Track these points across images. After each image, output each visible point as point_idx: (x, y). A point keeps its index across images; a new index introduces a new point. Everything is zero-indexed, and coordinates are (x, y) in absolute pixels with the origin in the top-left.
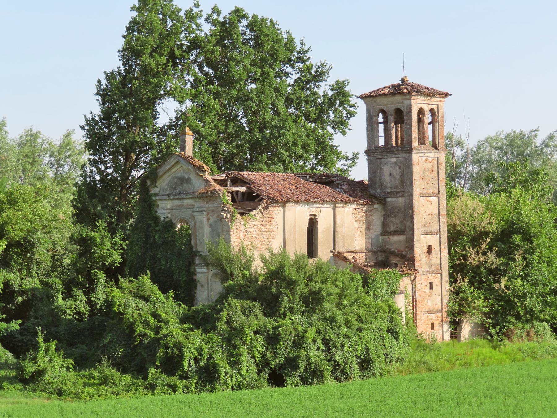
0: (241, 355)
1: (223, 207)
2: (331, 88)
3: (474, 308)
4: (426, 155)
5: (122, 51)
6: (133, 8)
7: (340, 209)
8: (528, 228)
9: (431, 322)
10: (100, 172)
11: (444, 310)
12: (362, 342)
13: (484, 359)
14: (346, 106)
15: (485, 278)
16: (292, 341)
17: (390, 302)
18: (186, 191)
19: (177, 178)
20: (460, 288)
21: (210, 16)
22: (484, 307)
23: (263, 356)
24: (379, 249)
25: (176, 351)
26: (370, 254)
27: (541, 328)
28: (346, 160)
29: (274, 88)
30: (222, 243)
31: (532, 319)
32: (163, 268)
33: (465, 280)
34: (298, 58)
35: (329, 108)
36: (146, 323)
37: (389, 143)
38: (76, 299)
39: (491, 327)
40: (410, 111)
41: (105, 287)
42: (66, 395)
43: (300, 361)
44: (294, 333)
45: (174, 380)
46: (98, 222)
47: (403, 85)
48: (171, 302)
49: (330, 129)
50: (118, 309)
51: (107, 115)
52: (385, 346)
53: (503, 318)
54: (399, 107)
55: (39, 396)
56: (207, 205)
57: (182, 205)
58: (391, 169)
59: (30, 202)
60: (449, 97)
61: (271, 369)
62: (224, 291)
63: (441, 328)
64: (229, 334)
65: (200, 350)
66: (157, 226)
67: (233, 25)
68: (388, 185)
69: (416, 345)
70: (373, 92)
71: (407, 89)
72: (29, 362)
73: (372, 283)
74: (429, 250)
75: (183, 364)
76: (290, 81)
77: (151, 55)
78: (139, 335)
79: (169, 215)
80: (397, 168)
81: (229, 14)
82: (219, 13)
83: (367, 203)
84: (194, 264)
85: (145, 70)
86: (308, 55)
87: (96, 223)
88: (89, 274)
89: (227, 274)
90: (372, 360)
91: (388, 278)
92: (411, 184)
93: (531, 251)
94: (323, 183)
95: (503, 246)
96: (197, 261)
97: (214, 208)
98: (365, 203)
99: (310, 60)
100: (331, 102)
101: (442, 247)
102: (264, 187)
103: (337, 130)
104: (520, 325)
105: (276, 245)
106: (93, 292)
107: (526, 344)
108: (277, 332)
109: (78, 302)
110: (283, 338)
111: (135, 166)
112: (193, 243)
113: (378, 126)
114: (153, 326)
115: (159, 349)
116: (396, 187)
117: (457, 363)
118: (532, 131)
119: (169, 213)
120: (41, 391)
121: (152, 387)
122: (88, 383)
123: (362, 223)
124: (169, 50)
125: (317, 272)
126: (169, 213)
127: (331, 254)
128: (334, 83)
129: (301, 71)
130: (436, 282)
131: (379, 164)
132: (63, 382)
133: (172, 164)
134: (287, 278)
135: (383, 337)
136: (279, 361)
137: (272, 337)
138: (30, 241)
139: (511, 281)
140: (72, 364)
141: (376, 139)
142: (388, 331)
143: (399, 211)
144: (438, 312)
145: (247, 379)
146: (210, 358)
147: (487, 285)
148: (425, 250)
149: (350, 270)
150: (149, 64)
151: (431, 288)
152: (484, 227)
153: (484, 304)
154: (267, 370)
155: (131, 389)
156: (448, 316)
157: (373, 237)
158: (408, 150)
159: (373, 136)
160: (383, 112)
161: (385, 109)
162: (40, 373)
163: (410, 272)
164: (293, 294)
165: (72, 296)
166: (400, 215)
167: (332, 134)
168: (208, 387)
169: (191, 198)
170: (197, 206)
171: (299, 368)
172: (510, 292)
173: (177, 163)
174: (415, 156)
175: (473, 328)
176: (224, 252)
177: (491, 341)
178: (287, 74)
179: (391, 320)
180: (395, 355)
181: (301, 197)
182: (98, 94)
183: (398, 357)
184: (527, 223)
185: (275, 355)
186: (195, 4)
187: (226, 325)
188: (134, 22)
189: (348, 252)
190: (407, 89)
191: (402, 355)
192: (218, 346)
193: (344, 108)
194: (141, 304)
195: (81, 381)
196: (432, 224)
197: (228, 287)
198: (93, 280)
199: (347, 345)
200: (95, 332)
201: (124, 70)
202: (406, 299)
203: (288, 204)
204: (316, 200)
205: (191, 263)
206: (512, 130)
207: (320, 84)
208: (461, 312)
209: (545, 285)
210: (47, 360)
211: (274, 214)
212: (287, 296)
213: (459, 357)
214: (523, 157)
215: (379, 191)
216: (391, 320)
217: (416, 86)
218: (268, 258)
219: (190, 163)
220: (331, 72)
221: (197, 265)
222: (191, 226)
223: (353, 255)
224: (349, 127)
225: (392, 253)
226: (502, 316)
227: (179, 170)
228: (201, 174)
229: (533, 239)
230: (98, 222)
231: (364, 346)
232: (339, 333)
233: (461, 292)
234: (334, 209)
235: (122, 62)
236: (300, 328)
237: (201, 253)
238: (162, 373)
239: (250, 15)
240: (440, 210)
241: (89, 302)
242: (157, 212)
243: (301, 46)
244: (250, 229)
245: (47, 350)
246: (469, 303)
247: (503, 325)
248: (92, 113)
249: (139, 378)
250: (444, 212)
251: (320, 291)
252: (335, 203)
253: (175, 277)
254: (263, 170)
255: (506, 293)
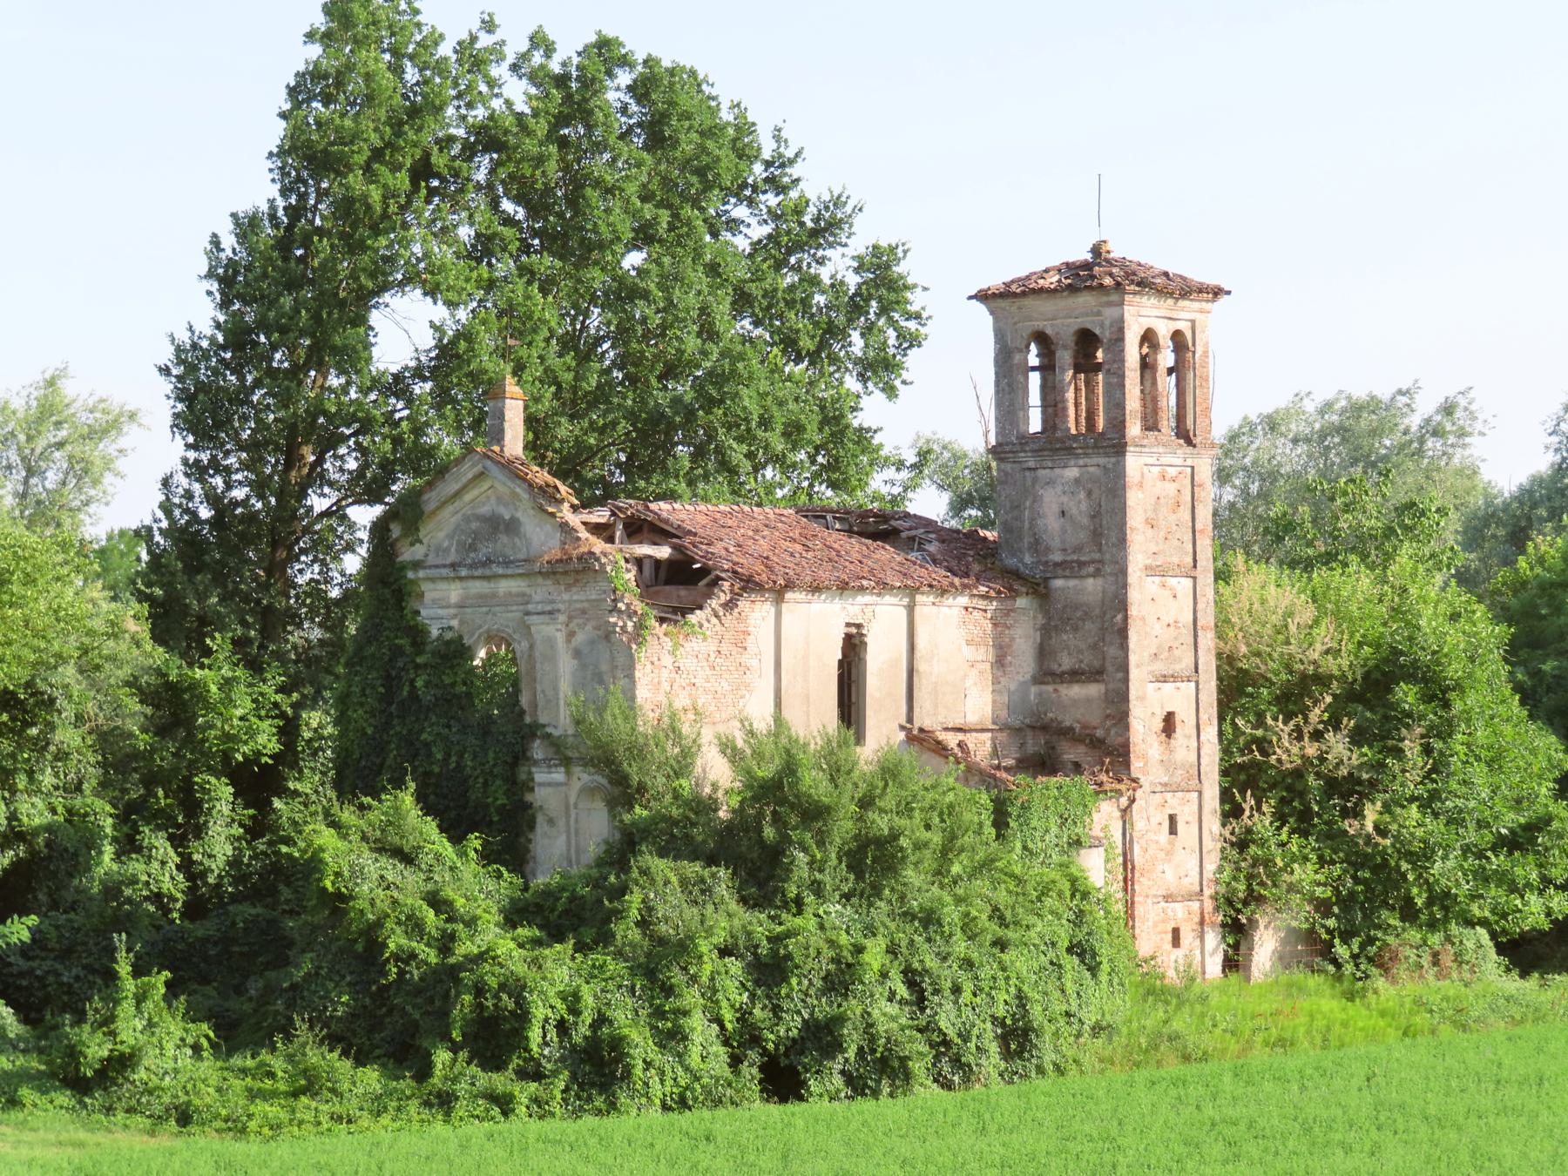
0: (686, 1013)
1: (614, 601)
2: (856, 264)
3: (1292, 888)
4: (1164, 460)
5: (278, 155)
6: (310, 36)
7: (926, 610)
8: (1439, 664)
9: (1172, 925)
10: (213, 499)
11: (1208, 892)
12: (1007, 978)
13: (1328, 1029)
14: (896, 316)
15: (1318, 803)
16: (823, 974)
17: (1073, 870)
18: (505, 556)
19: (479, 518)
20: (1249, 831)
21: (525, 57)
22: (1319, 884)
23: (743, 1016)
24: (1028, 721)
25: (508, 1002)
26: (1002, 736)
27: (1470, 945)
28: (898, 470)
29: (705, 266)
30: (614, 707)
31: (1446, 920)
32: (436, 769)
33: (1265, 808)
34: (766, 180)
35: (850, 320)
36: (414, 926)
37: (1060, 425)
38: (150, 857)
39: (1337, 941)
40: (1119, 338)
41: (229, 825)
42: (203, 1124)
43: (845, 1031)
44: (828, 953)
45: (500, 1081)
46: (213, 638)
47: (1099, 265)
48: (473, 865)
49: (852, 383)
50: (333, 883)
51: (237, 337)
52: (1063, 991)
53: (1365, 916)
54: (1089, 326)
55: (126, 1126)
56: (566, 597)
57: (494, 595)
58: (1065, 499)
59: (41, 582)
60: (1224, 300)
61: (765, 1052)
62: (618, 836)
63: (1198, 942)
64: (649, 955)
65: (573, 1001)
66: (420, 653)
67: (589, 84)
68: (1056, 543)
69: (1141, 990)
70: (1013, 282)
71: (1111, 275)
72: (94, 1031)
73: (1019, 816)
74: (1169, 724)
75: (527, 1038)
76: (742, 243)
77: (367, 168)
78: (396, 957)
79: (455, 623)
80: (1082, 495)
81: (579, 54)
82: (549, 50)
83: (999, 592)
84: (528, 759)
85: (347, 207)
86: (795, 171)
87: (208, 641)
88: (188, 781)
89: (629, 786)
90: (1034, 1030)
91: (1062, 801)
92: (1122, 541)
93: (1444, 731)
94: (876, 536)
95: (1368, 714)
96: (538, 750)
97: (586, 605)
98: (993, 594)
99: (801, 185)
100: (856, 306)
101: (1204, 717)
102: (720, 545)
103: (870, 384)
104: (1414, 935)
105: (761, 714)
106: (198, 837)
107: (1434, 988)
108: (782, 951)
109: (155, 865)
110: (797, 967)
111: (316, 477)
112: (524, 700)
113: (1027, 378)
114: (434, 932)
115: (458, 995)
116: (1078, 549)
117: (1259, 1038)
118: (1400, 392)
119: (454, 616)
120: (128, 1111)
121: (444, 1102)
122: (259, 1089)
123: (982, 650)
124: (418, 154)
125: (886, 785)
126: (454, 616)
127: (902, 736)
128: (862, 251)
129: (775, 216)
130: (1187, 813)
131: (1029, 482)
132: (189, 1086)
133: (464, 480)
134: (804, 800)
135: (1060, 966)
136: (788, 1030)
137: (766, 965)
138: (42, 693)
139: (1390, 812)
140: (207, 1037)
141: (1021, 414)
142: (1069, 950)
143: (1087, 615)
144: (1189, 897)
145: (705, 1080)
146: (601, 1020)
147: (1326, 823)
148: (1159, 724)
149: (957, 779)
150: (365, 197)
151: (1173, 830)
152: (1315, 662)
153: (1318, 877)
154: (753, 1055)
155: (385, 1108)
156: (1217, 909)
157: (1013, 688)
158: (1114, 446)
159: (1012, 404)
160: (1042, 339)
161: (1049, 331)
162: (122, 1063)
163: (1118, 786)
164: (821, 844)
165: (139, 849)
166: (1089, 625)
167: (858, 396)
168: (599, 1102)
169: (520, 575)
170: (537, 598)
171: (844, 1051)
172: (1388, 842)
173: (481, 476)
174: (1134, 463)
175: (1284, 942)
176: (624, 727)
177: (1339, 978)
178: (734, 225)
179: (1079, 918)
180: (1090, 1018)
181: (824, 574)
182: (210, 275)
183: (1097, 1022)
184: (1434, 653)
185: (776, 1015)
186: (483, 21)
187: (637, 931)
188: (315, 74)
189: (946, 729)
190: (1111, 275)
191: (1108, 1017)
192: (620, 987)
193: (892, 323)
194: (392, 869)
195: (237, 1084)
196: (1177, 652)
197: (633, 824)
198: (199, 803)
199: (968, 987)
200: (236, 949)
201: (285, 208)
202: (1107, 861)
203: (789, 595)
204: (865, 583)
205: (519, 757)
206: (1341, 392)
207: (829, 253)
208: (1253, 898)
209: (1482, 824)
210: (140, 1027)
211: (751, 621)
212: (805, 850)
213: (1260, 1021)
214: (1381, 468)
215: (1028, 559)
216: (1079, 918)
217: (1134, 267)
218: (740, 743)
219: (518, 476)
220: (858, 221)
221: (536, 763)
222: (518, 655)
223: (960, 736)
224: (905, 375)
225: (1066, 733)
226: (1362, 908)
227: (488, 497)
228: (551, 510)
229: (1452, 695)
230: (213, 638)
231: (1013, 990)
232: (949, 954)
233: (1254, 842)
234: (911, 609)
235: (278, 186)
236: (844, 939)
237: (549, 730)
238: (469, 1063)
239: (640, 57)
240: (1199, 615)
241: (186, 865)
242: (418, 613)
243: (775, 146)
244: (688, 663)
245: (140, 999)
246: (1275, 875)
247: (1368, 936)
248: (191, 329)
249: (404, 1077)
250: (1207, 618)
251: (894, 836)
252: (912, 591)
253: (474, 795)
254: (680, 497)
255: (1377, 844)
